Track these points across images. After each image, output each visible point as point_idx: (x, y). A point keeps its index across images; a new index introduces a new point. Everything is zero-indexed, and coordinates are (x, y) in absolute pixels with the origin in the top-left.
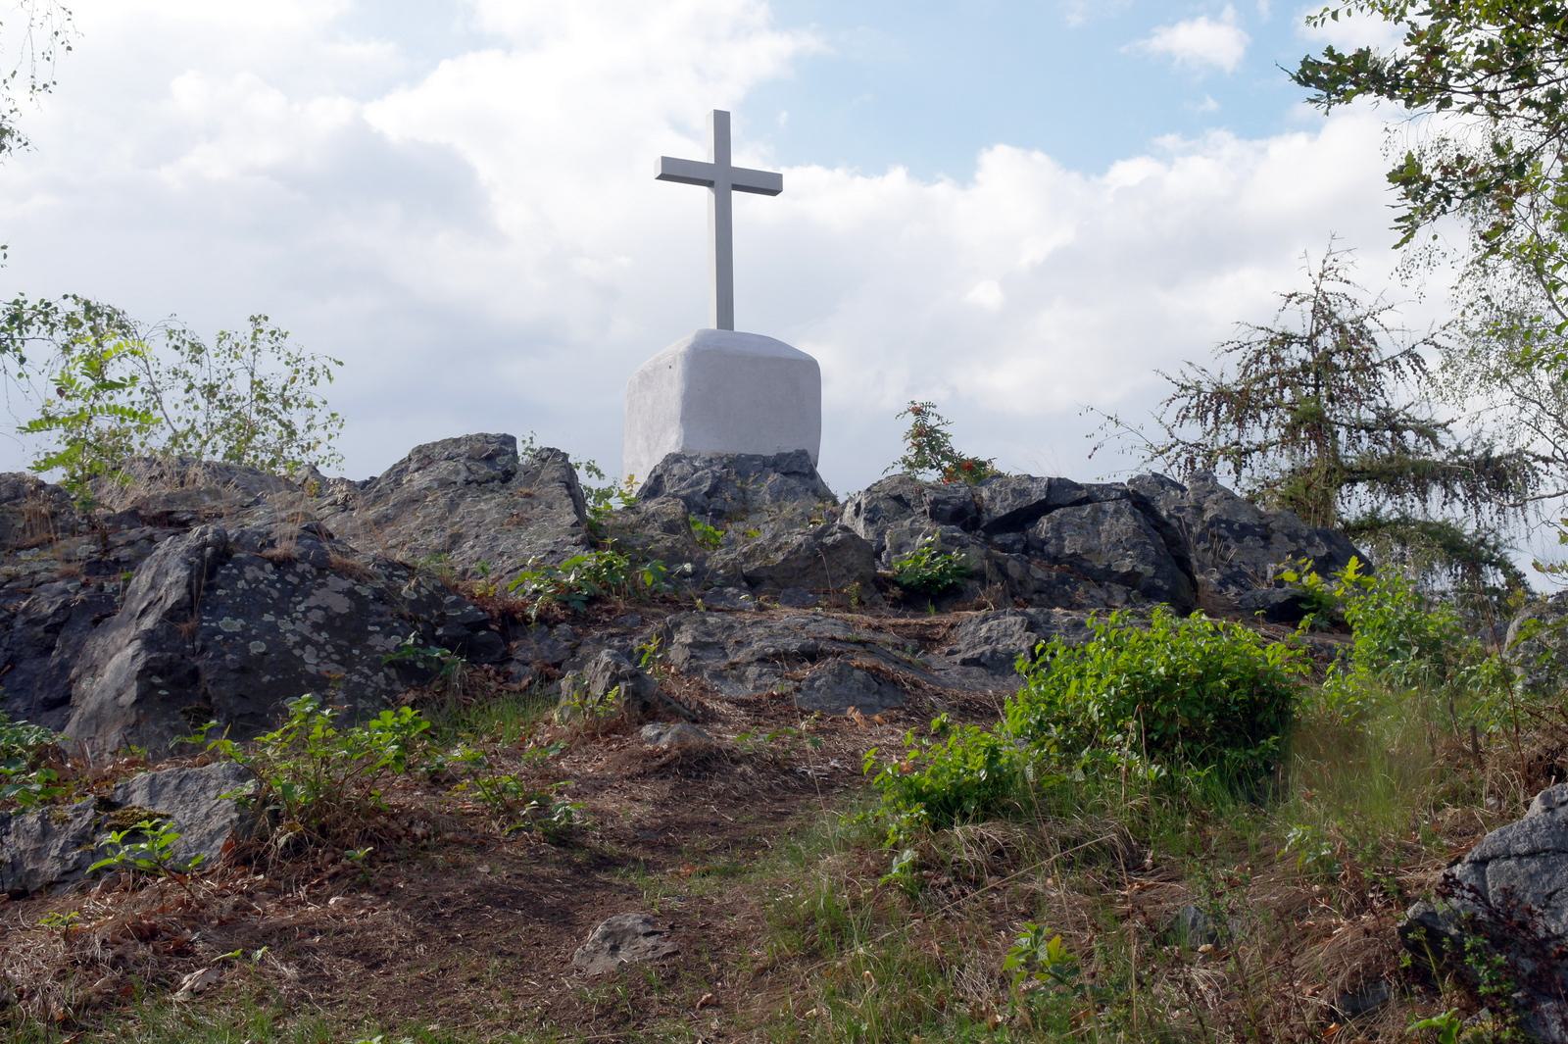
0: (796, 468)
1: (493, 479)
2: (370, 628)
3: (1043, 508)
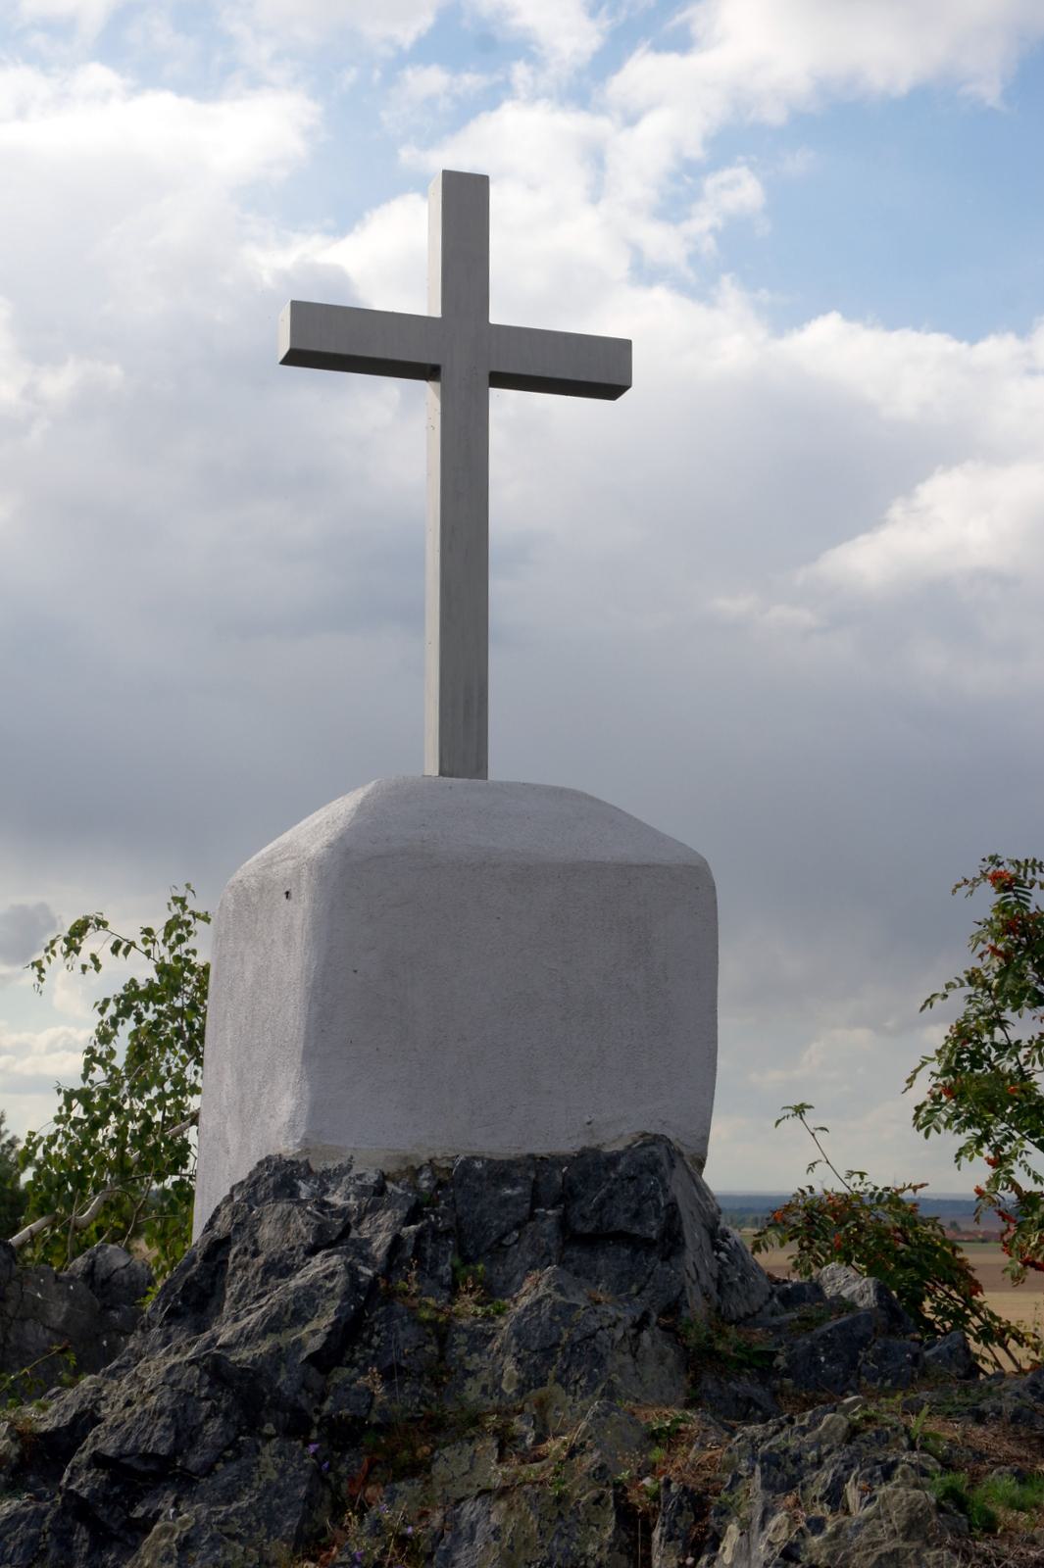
0: (621, 1222)
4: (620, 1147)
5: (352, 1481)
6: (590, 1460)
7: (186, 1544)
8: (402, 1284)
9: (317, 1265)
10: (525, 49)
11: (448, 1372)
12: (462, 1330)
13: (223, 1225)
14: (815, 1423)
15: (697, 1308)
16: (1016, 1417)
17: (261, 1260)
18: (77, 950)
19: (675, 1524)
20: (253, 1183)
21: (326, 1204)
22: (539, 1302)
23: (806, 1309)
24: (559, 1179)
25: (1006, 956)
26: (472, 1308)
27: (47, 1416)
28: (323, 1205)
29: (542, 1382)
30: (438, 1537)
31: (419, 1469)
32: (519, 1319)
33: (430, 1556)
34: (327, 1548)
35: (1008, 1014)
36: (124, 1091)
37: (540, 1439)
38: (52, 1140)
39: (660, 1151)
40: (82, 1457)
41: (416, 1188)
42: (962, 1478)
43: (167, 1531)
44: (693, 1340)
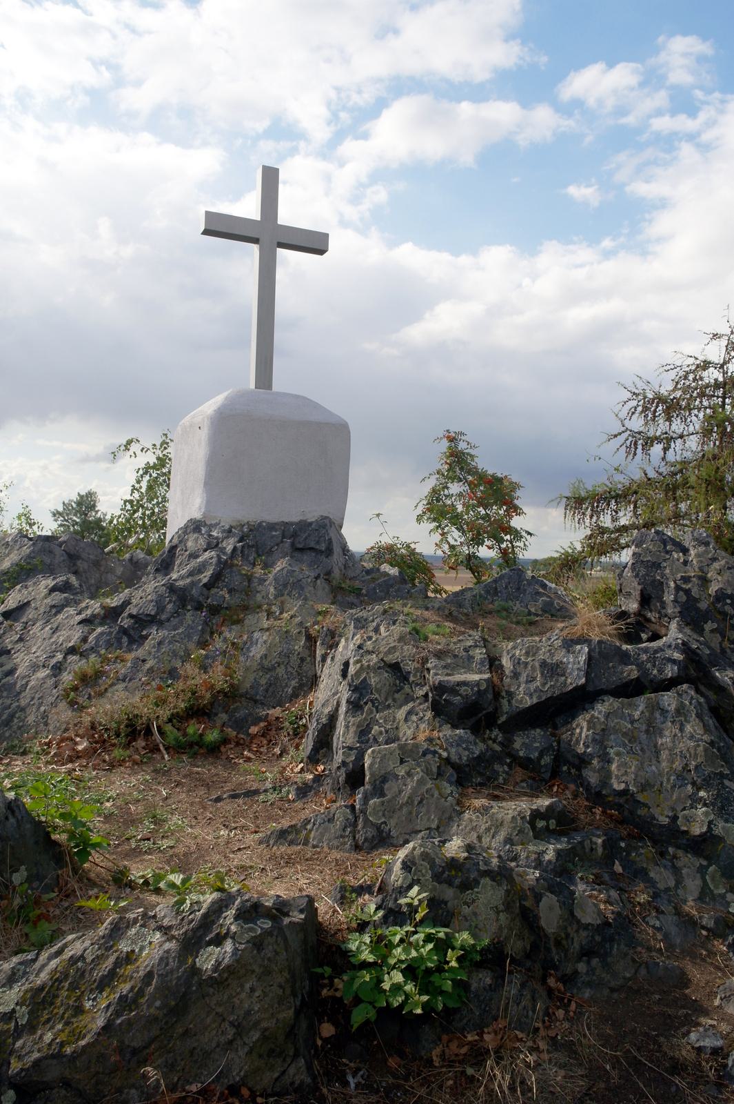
0: (312, 544)
4: (313, 520)
5: (217, 625)
6: (298, 619)
7: (160, 643)
8: (236, 562)
9: (207, 555)
10: (302, 136)
11: (251, 591)
12: (256, 577)
13: (175, 541)
14: (373, 609)
15: (337, 573)
16: (439, 609)
17: (188, 553)
18: (129, 450)
19: (324, 640)
20: (186, 527)
21: (211, 535)
22: (283, 569)
23: (373, 575)
24: (292, 530)
25: (450, 465)
26: (260, 571)
27: (113, 601)
28: (210, 536)
29: (283, 595)
30: (245, 643)
31: (239, 622)
32: (276, 574)
33: (242, 649)
34: (208, 646)
35: (449, 485)
36: (145, 500)
37: (281, 613)
38: (120, 516)
39: (327, 521)
40: (125, 614)
41: (243, 532)
42: (418, 625)
43: (153, 639)
44: (334, 583)
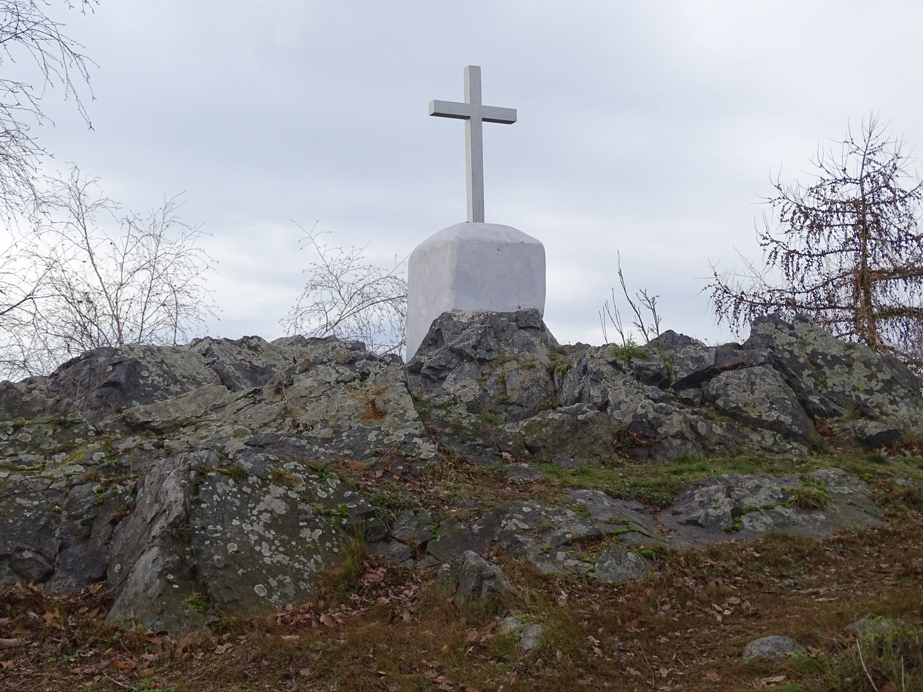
0: (532, 324)
1: (354, 379)
2: (301, 524)
3: (713, 372)
